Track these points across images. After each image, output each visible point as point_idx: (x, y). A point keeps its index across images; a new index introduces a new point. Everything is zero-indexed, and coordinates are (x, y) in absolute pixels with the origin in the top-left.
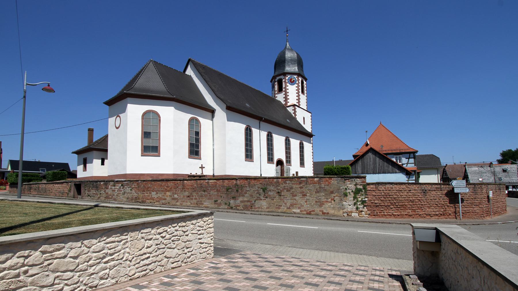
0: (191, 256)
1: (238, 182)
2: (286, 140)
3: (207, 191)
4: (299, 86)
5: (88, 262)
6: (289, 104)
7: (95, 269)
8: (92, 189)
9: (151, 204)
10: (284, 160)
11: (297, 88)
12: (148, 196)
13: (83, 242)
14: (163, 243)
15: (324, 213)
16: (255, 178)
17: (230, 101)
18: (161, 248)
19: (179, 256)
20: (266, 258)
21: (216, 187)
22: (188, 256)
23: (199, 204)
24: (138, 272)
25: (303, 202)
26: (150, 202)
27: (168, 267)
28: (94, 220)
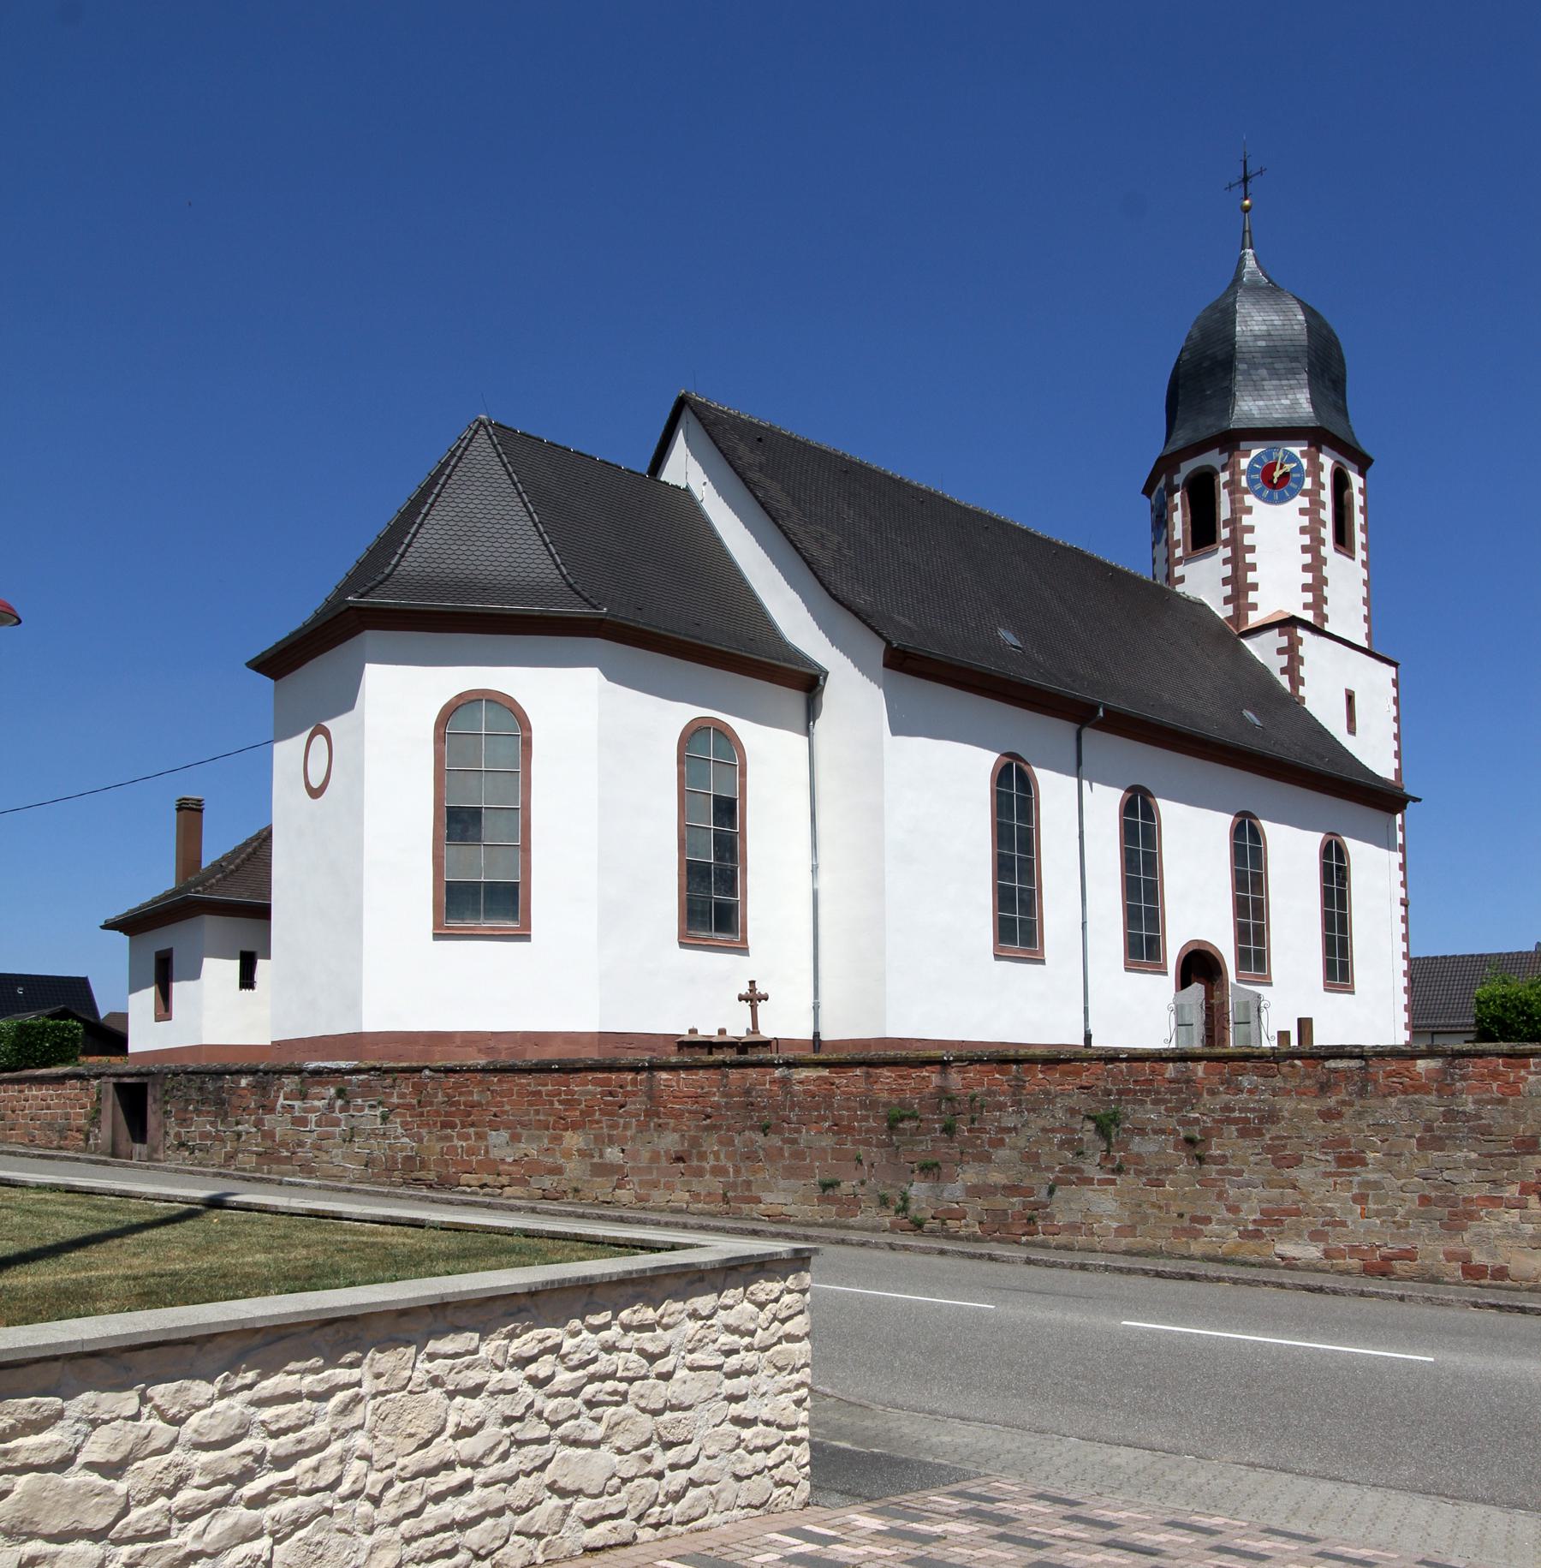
0: (686, 1489)
1: (955, 1079)
2: (1237, 832)
3: (779, 1131)
4: (1317, 504)
5: (171, 1494)
6: (1254, 619)
7: (204, 1531)
8: (198, 1112)
9: (485, 1195)
10: (1226, 946)
11: (1305, 521)
12: (471, 1151)
13: (149, 1392)
14: (540, 1415)
15: (1473, 1272)
16: (1054, 1059)
17: (905, 621)
18: (528, 1436)
19: (624, 1489)
20: (1110, 1526)
21: (830, 1106)
22: (672, 1488)
23: (736, 1198)
24: (412, 1560)
25: (1339, 1200)
26: (482, 1186)
27: (567, 1544)
28: (199, 1282)
